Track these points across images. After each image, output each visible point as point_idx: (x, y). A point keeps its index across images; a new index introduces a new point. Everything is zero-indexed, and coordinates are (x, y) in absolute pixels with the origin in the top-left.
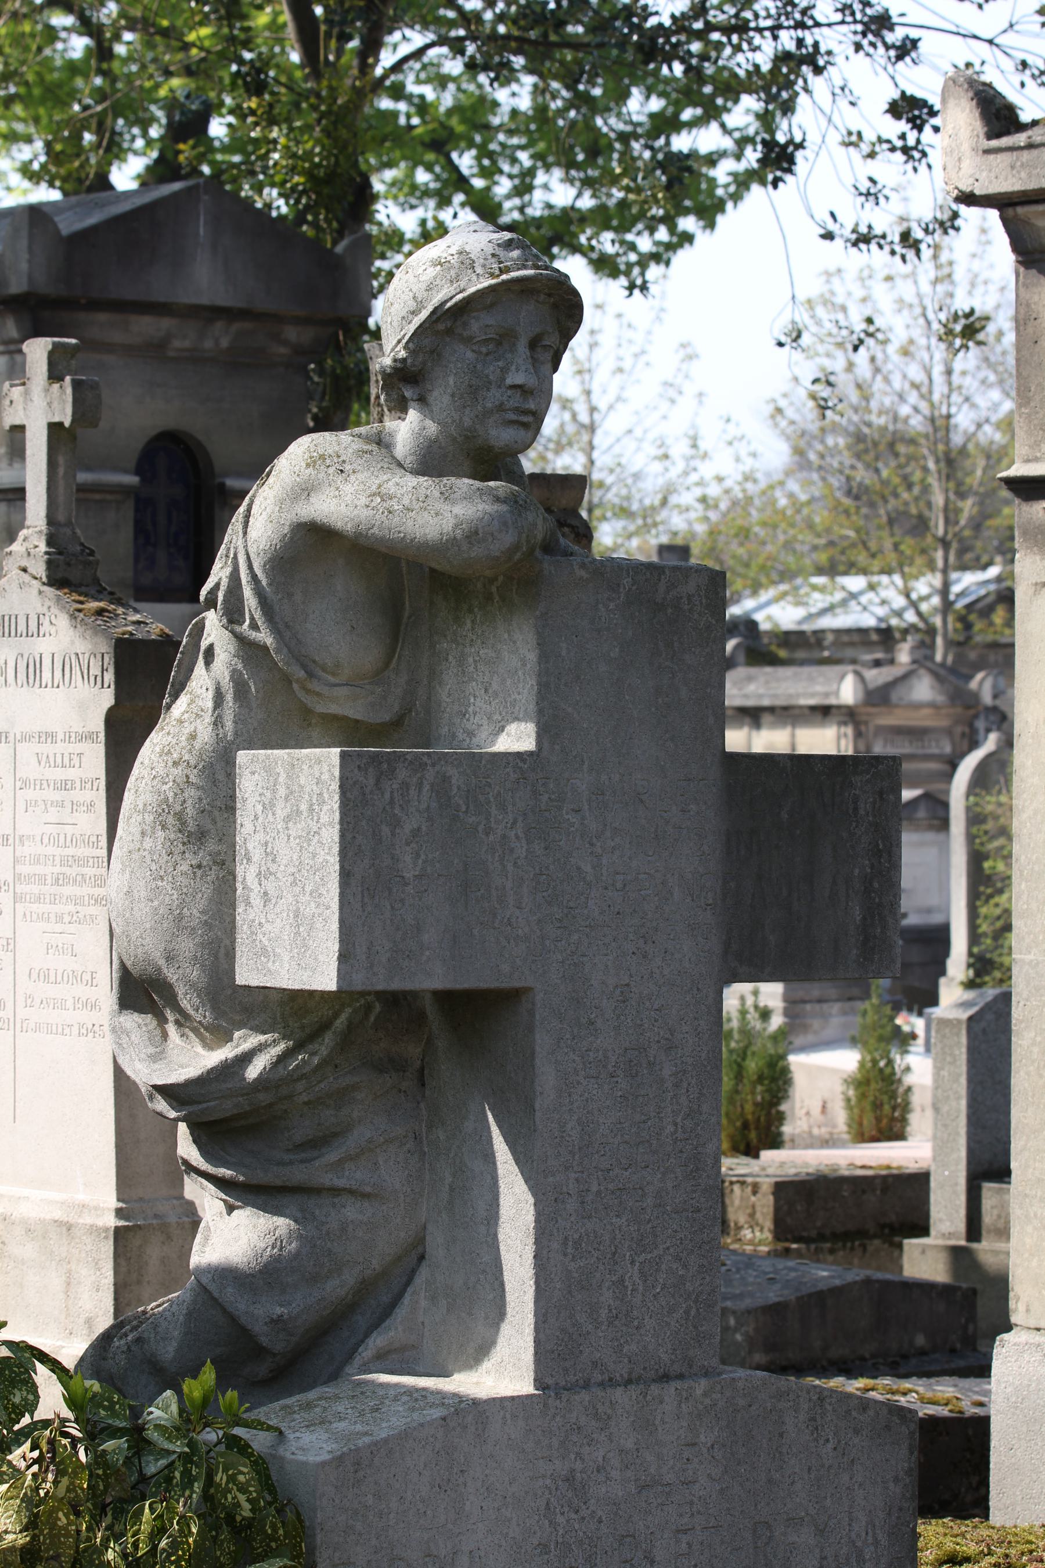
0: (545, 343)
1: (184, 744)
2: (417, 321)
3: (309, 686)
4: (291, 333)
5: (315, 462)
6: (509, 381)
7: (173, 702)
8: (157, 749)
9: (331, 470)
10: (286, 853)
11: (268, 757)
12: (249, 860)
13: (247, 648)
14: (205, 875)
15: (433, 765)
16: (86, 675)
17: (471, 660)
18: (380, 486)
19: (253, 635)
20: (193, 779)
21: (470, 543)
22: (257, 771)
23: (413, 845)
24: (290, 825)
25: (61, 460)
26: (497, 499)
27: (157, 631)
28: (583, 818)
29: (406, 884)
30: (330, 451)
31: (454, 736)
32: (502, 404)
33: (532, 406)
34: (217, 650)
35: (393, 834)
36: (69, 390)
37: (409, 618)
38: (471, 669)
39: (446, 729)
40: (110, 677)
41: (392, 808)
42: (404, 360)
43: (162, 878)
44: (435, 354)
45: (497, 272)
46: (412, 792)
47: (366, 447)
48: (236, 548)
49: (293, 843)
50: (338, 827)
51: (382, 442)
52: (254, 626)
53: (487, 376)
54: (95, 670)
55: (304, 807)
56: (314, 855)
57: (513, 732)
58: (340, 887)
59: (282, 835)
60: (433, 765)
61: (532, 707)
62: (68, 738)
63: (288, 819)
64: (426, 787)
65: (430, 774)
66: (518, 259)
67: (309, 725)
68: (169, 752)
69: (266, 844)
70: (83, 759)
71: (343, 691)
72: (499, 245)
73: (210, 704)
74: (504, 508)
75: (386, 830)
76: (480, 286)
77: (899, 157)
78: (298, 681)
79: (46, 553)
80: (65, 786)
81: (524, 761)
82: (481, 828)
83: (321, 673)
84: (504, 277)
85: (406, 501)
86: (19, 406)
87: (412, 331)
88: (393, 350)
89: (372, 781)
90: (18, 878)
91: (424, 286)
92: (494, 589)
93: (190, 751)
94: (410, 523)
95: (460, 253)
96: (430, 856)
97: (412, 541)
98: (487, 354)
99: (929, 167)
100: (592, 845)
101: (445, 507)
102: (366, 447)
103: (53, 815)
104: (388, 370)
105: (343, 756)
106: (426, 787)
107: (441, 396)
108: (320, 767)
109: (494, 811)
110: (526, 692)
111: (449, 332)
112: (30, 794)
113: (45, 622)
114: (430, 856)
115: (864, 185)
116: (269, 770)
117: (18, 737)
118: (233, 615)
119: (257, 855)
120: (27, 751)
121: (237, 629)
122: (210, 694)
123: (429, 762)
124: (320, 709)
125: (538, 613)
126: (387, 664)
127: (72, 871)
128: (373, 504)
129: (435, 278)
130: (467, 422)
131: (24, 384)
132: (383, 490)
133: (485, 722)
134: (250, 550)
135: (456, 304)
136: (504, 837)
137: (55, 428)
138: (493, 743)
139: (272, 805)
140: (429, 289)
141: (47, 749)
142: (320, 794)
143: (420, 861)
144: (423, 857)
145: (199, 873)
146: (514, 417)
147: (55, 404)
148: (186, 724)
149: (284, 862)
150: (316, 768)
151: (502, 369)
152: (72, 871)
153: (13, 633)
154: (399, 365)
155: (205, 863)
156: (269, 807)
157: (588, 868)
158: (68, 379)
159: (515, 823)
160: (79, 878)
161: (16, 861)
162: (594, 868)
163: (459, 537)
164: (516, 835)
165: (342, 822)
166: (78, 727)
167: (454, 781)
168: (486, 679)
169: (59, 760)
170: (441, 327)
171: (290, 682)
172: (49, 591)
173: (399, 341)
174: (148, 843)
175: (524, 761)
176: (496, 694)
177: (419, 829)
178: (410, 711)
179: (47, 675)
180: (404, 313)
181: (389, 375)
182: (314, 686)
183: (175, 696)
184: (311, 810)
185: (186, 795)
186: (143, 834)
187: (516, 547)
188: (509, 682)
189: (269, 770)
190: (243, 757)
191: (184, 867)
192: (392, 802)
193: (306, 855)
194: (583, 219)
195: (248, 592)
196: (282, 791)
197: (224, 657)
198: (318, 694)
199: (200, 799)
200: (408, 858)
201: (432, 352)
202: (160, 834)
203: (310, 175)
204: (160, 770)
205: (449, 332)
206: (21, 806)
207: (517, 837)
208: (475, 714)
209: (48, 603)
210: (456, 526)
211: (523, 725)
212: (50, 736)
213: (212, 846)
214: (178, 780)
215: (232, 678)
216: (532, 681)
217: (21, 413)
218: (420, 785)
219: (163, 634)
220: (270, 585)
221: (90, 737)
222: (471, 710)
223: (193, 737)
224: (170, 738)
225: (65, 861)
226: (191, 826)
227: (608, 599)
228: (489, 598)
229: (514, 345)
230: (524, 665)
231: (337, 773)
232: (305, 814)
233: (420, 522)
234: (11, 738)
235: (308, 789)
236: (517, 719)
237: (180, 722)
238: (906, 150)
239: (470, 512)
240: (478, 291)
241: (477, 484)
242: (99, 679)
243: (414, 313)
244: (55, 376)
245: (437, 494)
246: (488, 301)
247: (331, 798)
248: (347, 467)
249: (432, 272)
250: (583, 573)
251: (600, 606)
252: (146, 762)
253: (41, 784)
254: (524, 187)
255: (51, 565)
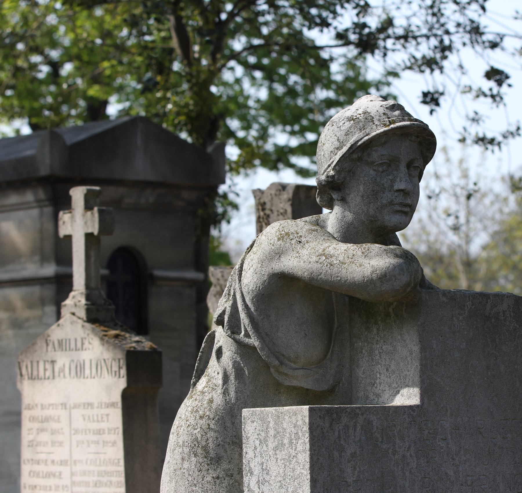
0: (415, 165)
1: (206, 406)
2: (340, 154)
3: (281, 370)
4: (186, 195)
5: (283, 237)
6: (396, 187)
7: (197, 381)
8: (190, 409)
9: (293, 242)
10: (275, 469)
11: (262, 412)
12: (252, 473)
13: (243, 348)
14: (221, 483)
15: (362, 414)
16: (110, 371)
17: (377, 352)
18: (324, 250)
19: (247, 340)
20: (212, 426)
21: (381, 282)
22: (255, 422)
23: (352, 462)
24: (278, 452)
25: (92, 253)
26: (396, 256)
27: (149, 346)
28: (448, 444)
29: (349, 486)
30: (292, 231)
31: (367, 397)
32: (392, 201)
33: (409, 202)
34: (224, 350)
35: (340, 456)
36: (96, 215)
37: (337, 328)
38: (377, 357)
39: (362, 393)
40: (123, 372)
41: (340, 441)
42: (333, 176)
43: (195, 485)
44: (351, 172)
45: (388, 123)
46: (350, 431)
47: (313, 228)
48: (234, 289)
49: (280, 463)
50: (308, 453)
51: (320, 225)
52: (247, 335)
53: (383, 185)
54: (115, 368)
55: (286, 441)
56: (294, 470)
57: (405, 394)
58: (311, 489)
59: (272, 458)
60: (362, 414)
61: (417, 379)
62: (100, 406)
63: (276, 449)
64: (359, 428)
65: (361, 420)
66: (399, 116)
67: (280, 393)
68: (197, 411)
69: (262, 464)
70: (110, 417)
71: (301, 372)
72: (387, 108)
73: (220, 382)
74: (401, 261)
75: (336, 454)
76: (378, 132)
77: (489, 100)
78: (274, 367)
79: (86, 305)
80: (99, 432)
81: (414, 411)
82: (390, 451)
83: (287, 362)
84: (392, 126)
85: (341, 258)
86: (68, 225)
87: (337, 159)
88: (325, 171)
89: (327, 425)
90: (73, 483)
91: (343, 133)
92: (391, 310)
93: (210, 410)
94: (344, 271)
95: (365, 113)
96: (362, 469)
97: (345, 281)
98: (383, 172)
99: (505, 105)
100: (453, 459)
101: (366, 261)
102: (313, 228)
103: (93, 448)
104: (323, 183)
105: (310, 410)
106: (359, 428)
107: (355, 197)
108: (296, 418)
109: (397, 441)
110: (413, 369)
111: (360, 159)
112: (80, 437)
113: (86, 342)
114: (362, 469)
115: (472, 115)
116: (263, 420)
117: (72, 406)
118: (234, 328)
119: (257, 470)
120: (77, 413)
121: (237, 337)
122: (220, 376)
123: (360, 413)
124: (287, 383)
125: (419, 323)
126: (326, 356)
127: (104, 479)
128: (321, 261)
129: (350, 128)
130: (372, 212)
131: (71, 212)
132: (326, 252)
133: (387, 388)
134: (243, 290)
135: (364, 142)
136: (404, 456)
137: (89, 236)
138: (392, 400)
139: (266, 441)
140: (347, 134)
141: (88, 412)
142: (297, 433)
143: (356, 472)
144: (358, 469)
145: (218, 482)
146: (398, 208)
147: (89, 223)
148: (206, 394)
149: (274, 474)
150: (294, 418)
151: (391, 180)
152: (104, 479)
153: (68, 349)
154: (330, 179)
155: (221, 476)
156: (263, 442)
157: (451, 473)
158: (96, 209)
159: (409, 448)
160: (108, 483)
161: (72, 474)
162: (455, 473)
163: (374, 278)
164: (410, 454)
165: (311, 450)
166: (105, 399)
167: (374, 424)
168: (387, 363)
169: (95, 418)
170: (355, 156)
171: (269, 368)
172: (88, 325)
173: (329, 166)
174: (186, 465)
175: (414, 411)
176: (394, 372)
177: (355, 453)
178: (339, 383)
179: (87, 372)
180: (332, 149)
181: (324, 185)
182: (283, 369)
183: (198, 378)
184: (291, 443)
185: (208, 436)
186: (183, 459)
187: (408, 284)
188: (402, 364)
189: (263, 420)
190: (246, 412)
191: (209, 478)
192: (339, 437)
193: (288, 470)
194: (293, 151)
195: (243, 315)
196: (272, 432)
197: (227, 355)
198: (286, 375)
199: (217, 438)
200: (349, 470)
201: (350, 171)
202: (193, 459)
203: (188, 115)
204: (192, 421)
205: (360, 159)
206: (74, 443)
207: (411, 456)
208: (380, 384)
209: (87, 332)
210: (373, 272)
211: (411, 390)
212: (89, 405)
213: (225, 465)
214: (204, 427)
215: (234, 366)
216: (416, 364)
217: (69, 228)
218: (355, 427)
219: (151, 348)
220: (256, 310)
221: (113, 405)
222: (377, 381)
223: (211, 401)
224: (197, 403)
225: (100, 474)
226: (212, 454)
227: (459, 314)
228: (388, 315)
229: (398, 166)
230: (411, 354)
231: (307, 420)
232: (287, 445)
233: (350, 270)
234: (68, 407)
235: (288, 431)
236: (407, 386)
237: (203, 393)
238: (493, 97)
239: (381, 263)
240: (377, 134)
241: (384, 247)
242: (117, 373)
243: (338, 149)
244: (88, 207)
245: (360, 253)
246: (383, 140)
247: (304, 435)
248: (303, 239)
249: (348, 124)
250: (444, 299)
251: (454, 318)
252: (183, 417)
253: (86, 431)
254: (264, 136)
255: (88, 311)
